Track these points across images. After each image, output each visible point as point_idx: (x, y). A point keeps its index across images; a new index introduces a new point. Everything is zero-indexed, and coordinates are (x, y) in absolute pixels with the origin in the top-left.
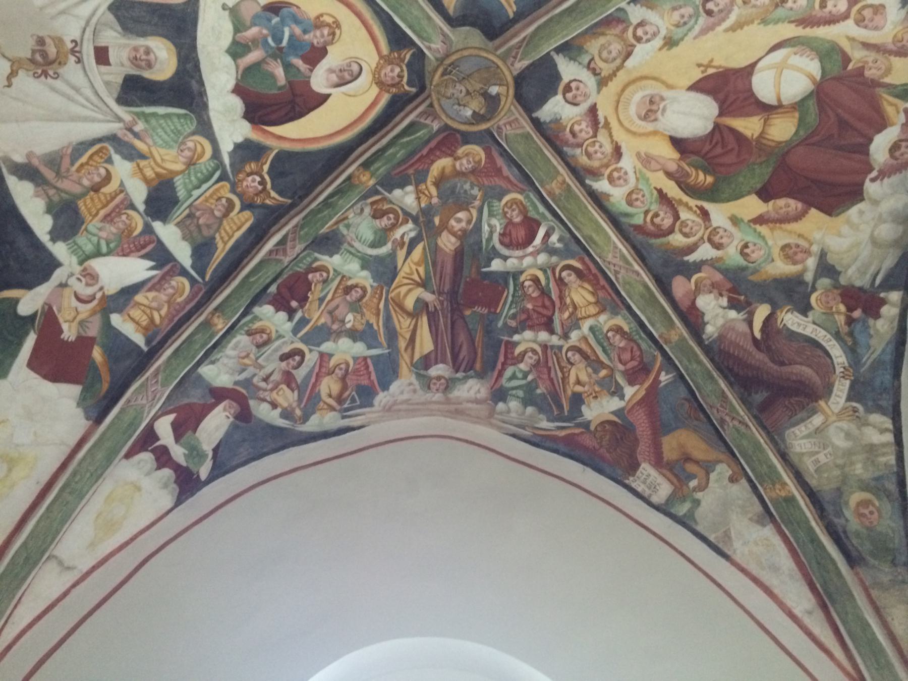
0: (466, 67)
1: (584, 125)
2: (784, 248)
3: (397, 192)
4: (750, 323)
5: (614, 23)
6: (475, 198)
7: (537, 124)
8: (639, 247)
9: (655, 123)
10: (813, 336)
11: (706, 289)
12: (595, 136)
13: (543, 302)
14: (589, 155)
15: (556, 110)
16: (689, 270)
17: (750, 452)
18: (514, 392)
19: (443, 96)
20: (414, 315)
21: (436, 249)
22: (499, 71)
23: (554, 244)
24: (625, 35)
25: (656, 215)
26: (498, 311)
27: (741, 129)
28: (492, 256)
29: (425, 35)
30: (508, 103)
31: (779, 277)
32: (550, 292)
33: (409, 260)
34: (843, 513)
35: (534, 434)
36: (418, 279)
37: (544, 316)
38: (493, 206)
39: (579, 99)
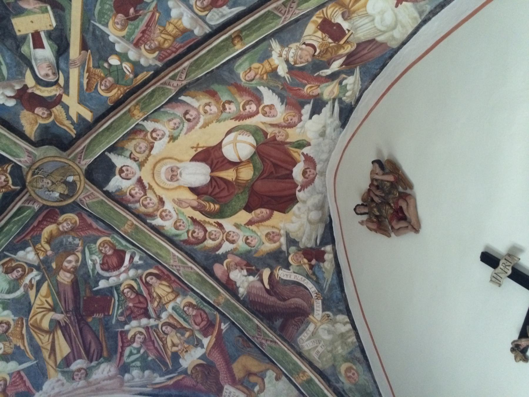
0: (48, 169)
1: (137, 190)
2: (267, 235)
3: (21, 253)
4: (262, 281)
5: (138, 132)
6: (78, 245)
7: (108, 194)
8: (189, 252)
9: (177, 182)
10: (295, 280)
11: (233, 267)
12: (145, 194)
13: (139, 300)
14: (145, 206)
15: (117, 184)
16: (221, 259)
17: (281, 359)
18: (134, 364)
19: (36, 188)
20: (51, 331)
21: (58, 284)
22: (71, 167)
23: (137, 262)
24: (146, 138)
25: (194, 232)
26: (110, 313)
27: (225, 177)
28: (98, 279)
29: (14, 154)
30: (83, 184)
31: (269, 252)
32: (143, 293)
33: (39, 296)
34: (339, 379)
35: (154, 388)
36: (48, 307)
37: (141, 308)
38: (91, 248)
39: (130, 176)
